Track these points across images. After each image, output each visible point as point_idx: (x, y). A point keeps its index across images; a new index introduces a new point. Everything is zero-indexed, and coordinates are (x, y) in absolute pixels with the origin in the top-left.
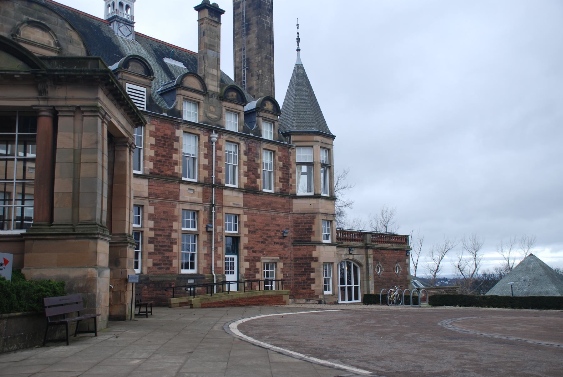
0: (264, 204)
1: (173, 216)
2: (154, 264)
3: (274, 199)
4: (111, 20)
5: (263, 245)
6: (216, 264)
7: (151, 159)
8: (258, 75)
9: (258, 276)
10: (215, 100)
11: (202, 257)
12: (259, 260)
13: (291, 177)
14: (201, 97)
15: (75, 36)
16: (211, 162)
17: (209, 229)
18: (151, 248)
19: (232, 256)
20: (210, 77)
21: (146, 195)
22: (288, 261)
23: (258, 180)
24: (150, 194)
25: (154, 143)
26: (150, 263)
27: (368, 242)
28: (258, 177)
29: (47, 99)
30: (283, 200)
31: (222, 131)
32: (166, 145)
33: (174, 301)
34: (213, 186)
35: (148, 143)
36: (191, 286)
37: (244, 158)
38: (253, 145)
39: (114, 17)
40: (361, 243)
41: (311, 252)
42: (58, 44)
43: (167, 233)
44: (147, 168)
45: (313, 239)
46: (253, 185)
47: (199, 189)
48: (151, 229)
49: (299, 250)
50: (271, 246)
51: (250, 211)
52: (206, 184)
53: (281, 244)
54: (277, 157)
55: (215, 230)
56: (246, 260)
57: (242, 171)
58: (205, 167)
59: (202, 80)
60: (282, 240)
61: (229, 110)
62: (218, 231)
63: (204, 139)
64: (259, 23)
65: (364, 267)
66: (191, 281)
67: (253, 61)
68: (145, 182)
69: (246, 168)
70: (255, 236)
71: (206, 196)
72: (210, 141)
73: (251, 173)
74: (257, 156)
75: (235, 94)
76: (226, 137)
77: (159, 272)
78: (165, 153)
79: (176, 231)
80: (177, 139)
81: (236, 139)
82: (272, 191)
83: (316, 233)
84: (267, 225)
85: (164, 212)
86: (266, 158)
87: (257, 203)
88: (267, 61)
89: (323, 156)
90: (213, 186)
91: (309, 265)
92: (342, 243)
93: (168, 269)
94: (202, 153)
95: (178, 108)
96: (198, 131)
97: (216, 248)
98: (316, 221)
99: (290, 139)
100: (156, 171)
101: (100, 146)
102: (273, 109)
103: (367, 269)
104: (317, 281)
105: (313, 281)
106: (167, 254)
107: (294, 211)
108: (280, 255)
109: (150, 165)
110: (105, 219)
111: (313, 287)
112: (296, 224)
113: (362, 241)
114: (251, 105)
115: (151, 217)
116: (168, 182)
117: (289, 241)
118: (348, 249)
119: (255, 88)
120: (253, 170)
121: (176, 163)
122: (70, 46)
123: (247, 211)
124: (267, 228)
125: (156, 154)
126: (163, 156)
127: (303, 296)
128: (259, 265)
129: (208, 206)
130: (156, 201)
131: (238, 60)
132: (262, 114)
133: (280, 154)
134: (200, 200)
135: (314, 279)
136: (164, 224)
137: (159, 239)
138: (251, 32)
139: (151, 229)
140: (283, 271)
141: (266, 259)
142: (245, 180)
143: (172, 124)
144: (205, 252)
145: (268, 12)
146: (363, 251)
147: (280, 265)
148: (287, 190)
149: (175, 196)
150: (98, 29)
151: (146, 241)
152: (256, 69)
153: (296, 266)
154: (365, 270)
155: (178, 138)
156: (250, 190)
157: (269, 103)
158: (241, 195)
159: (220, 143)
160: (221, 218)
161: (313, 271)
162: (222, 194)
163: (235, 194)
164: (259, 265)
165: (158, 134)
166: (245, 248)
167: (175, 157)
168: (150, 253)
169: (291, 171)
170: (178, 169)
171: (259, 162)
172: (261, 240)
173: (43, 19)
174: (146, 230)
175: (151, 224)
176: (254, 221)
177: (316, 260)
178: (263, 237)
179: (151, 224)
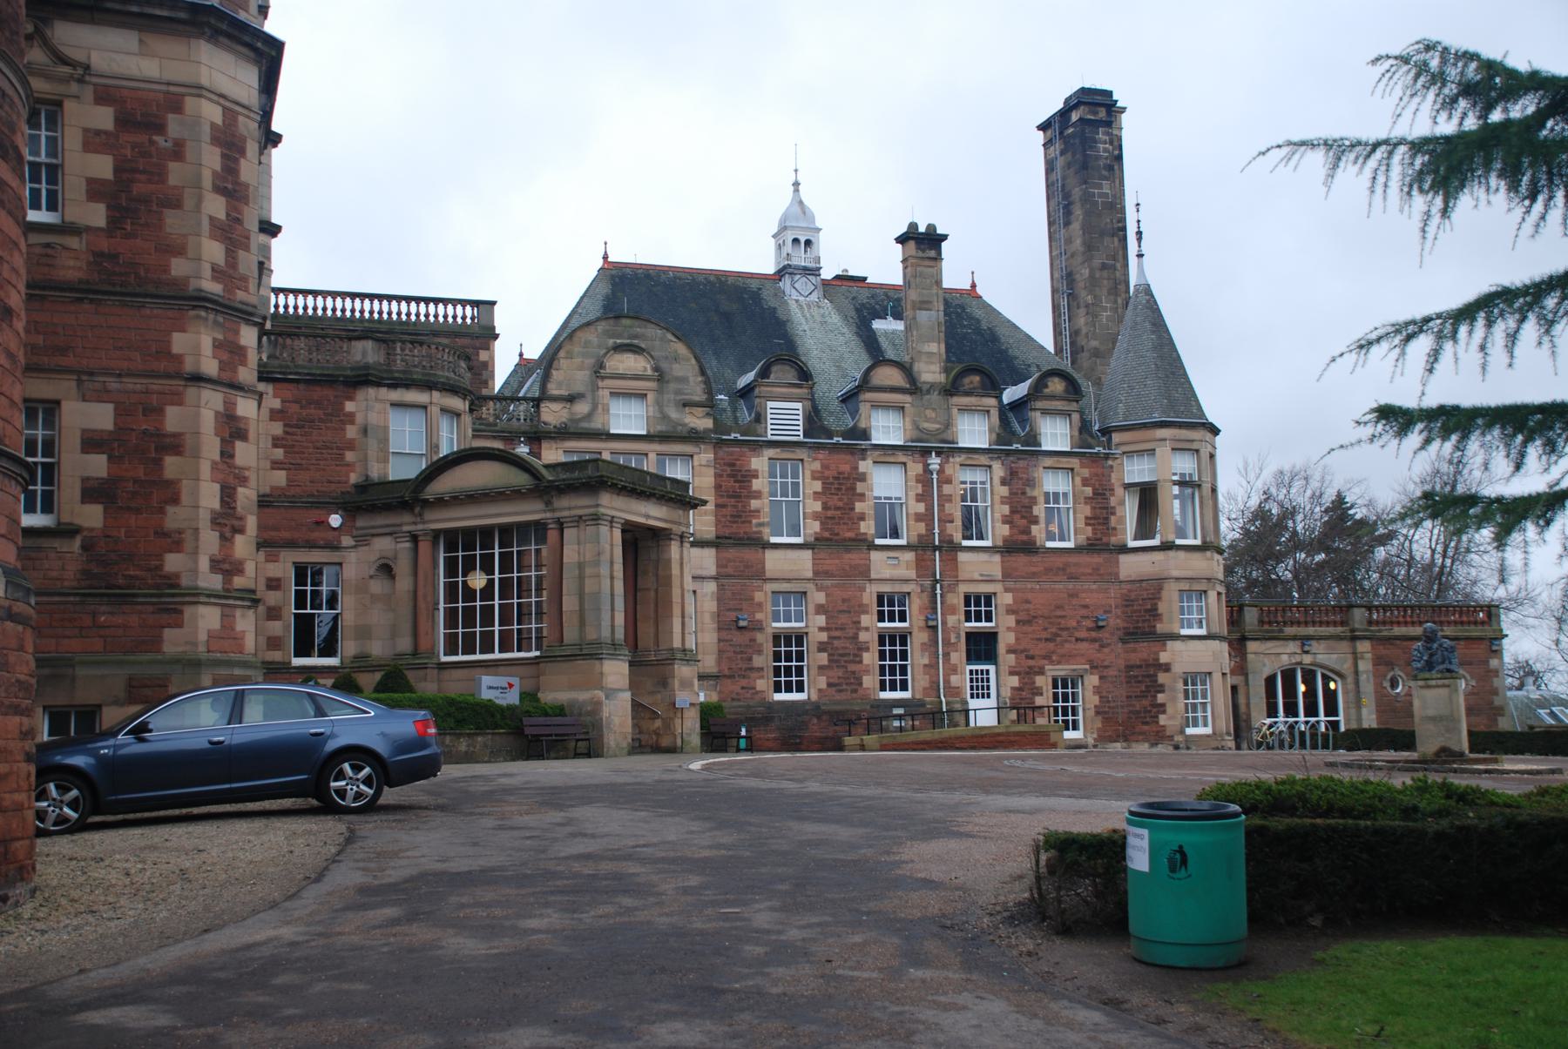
0: (1048, 570)
1: (861, 605)
2: (830, 685)
3: (1073, 559)
4: (781, 273)
5: (1051, 646)
6: (947, 681)
7: (816, 516)
8: (1087, 306)
9: (1039, 701)
10: (935, 397)
11: (919, 670)
12: (1041, 672)
13: (1114, 514)
14: (908, 398)
15: (681, 349)
16: (930, 508)
17: (931, 623)
18: (823, 658)
19: (985, 667)
20: (924, 358)
21: (810, 574)
22: (1112, 672)
23: (1034, 527)
24: (816, 573)
25: (819, 489)
26: (822, 682)
27: (1357, 626)
28: (1035, 521)
29: (553, 510)
30: (1096, 559)
31: (949, 450)
32: (842, 490)
33: (848, 740)
34: (935, 548)
35: (809, 492)
36: (900, 717)
37: (1004, 491)
38: (1022, 464)
39: (785, 267)
40: (1340, 629)
41: (1157, 653)
42: (656, 369)
43: (851, 633)
44: (809, 531)
45: (1160, 628)
46: (1024, 537)
47: (909, 556)
48: (821, 629)
49: (1134, 651)
50: (1067, 645)
51: (1018, 585)
52: (923, 547)
53: (1094, 640)
54: (1078, 480)
55: (944, 623)
56: (1012, 673)
57: (998, 516)
58: (919, 518)
59: (906, 369)
60: (1094, 634)
61: (964, 410)
62: (950, 624)
63: (916, 468)
64: (1087, 198)
65: (1350, 679)
66: (900, 711)
67: (1077, 277)
68: (807, 555)
69: (1006, 509)
70: (1030, 629)
71: (923, 567)
72: (927, 470)
73: (1017, 517)
74: (1031, 483)
75: (976, 379)
76: (959, 459)
77: (838, 697)
78: (840, 504)
79: (867, 629)
80: (863, 478)
81: (983, 460)
82: (1070, 544)
83: (1165, 618)
84: (1058, 607)
85: (844, 601)
86: (1054, 483)
87: (1034, 569)
88: (1105, 273)
89: (1184, 465)
90: (935, 548)
91: (1154, 678)
92: (1281, 631)
93: (855, 691)
94: (912, 494)
95: (863, 425)
96: (902, 458)
97: (946, 655)
98: (1165, 594)
99: (1110, 439)
100: (827, 534)
101: (606, 557)
102: (1066, 391)
103: (1357, 683)
104: (1169, 710)
105: (1162, 708)
106: (852, 667)
107: (1122, 578)
108: (1090, 662)
109: (815, 527)
110: (620, 635)
111: (1163, 720)
112: (1128, 602)
113: (1342, 623)
114: (1011, 394)
115: (820, 609)
116: (848, 551)
117: (1112, 634)
118: (1298, 643)
119: (1084, 331)
120: (1021, 509)
121: (862, 517)
122: (676, 366)
123: (1011, 585)
124: (1059, 613)
125: (825, 507)
126: (838, 508)
127: (1145, 737)
128: (1040, 681)
129: (928, 583)
130: (829, 583)
131: (1056, 275)
132: (1039, 404)
133: (1086, 472)
134: (912, 574)
135: (1163, 705)
136: (844, 619)
137: (836, 643)
138: (1072, 217)
139: (821, 629)
140: (1097, 691)
141: (1054, 670)
142: (1005, 530)
143: (852, 454)
144: (926, 661)
145: (1105, 173)
146: (1345, 646)
147: (1093, 680)
148: (1105, 540)
149: (864, 573)
150: (756, 296)
151: (814, 648)
152: (1083, 293)
153: (1130, 680)
154: (1351, 686)
155: (864, 474)
156: (1018, 547)
157: (1056, 380)
158: (997, 558)
159: (949, 470)
160: (955, 601)
161: (1161, 689)
162: (955, 559)
163: (983, 557)
164: (1040, 681)
165: (827, 473)
166: (1009, 651)
167: (859, 507)
168: (821, 668)
169: (1113, 501)
170: (867, 527)
171: (1035, 493)
172: (1045, 635)
173: (636, 337)
174: (813, 631)
175: (821, 620)
176: (1028, 602)
177: (1167, 668)
178: (1048, 631)
179: (821, 620)
